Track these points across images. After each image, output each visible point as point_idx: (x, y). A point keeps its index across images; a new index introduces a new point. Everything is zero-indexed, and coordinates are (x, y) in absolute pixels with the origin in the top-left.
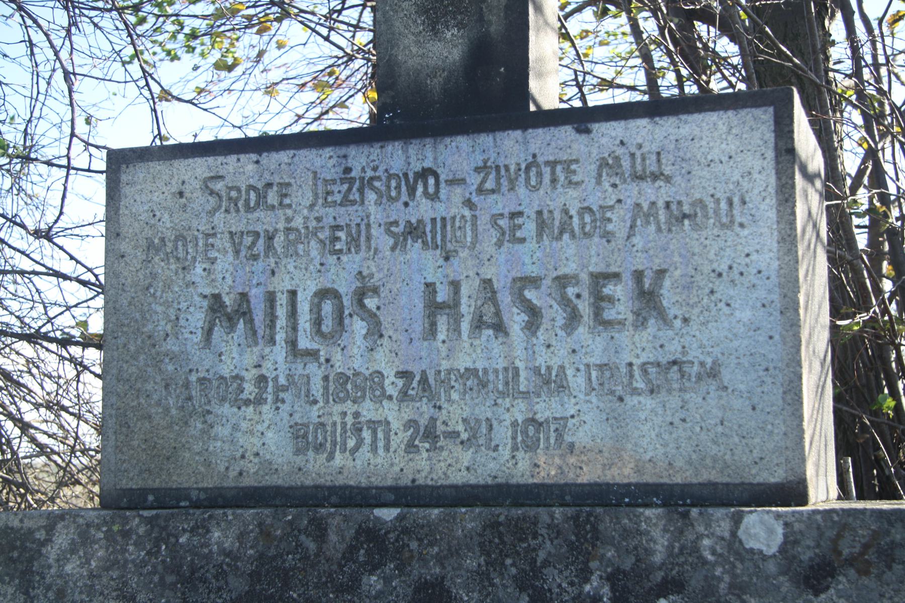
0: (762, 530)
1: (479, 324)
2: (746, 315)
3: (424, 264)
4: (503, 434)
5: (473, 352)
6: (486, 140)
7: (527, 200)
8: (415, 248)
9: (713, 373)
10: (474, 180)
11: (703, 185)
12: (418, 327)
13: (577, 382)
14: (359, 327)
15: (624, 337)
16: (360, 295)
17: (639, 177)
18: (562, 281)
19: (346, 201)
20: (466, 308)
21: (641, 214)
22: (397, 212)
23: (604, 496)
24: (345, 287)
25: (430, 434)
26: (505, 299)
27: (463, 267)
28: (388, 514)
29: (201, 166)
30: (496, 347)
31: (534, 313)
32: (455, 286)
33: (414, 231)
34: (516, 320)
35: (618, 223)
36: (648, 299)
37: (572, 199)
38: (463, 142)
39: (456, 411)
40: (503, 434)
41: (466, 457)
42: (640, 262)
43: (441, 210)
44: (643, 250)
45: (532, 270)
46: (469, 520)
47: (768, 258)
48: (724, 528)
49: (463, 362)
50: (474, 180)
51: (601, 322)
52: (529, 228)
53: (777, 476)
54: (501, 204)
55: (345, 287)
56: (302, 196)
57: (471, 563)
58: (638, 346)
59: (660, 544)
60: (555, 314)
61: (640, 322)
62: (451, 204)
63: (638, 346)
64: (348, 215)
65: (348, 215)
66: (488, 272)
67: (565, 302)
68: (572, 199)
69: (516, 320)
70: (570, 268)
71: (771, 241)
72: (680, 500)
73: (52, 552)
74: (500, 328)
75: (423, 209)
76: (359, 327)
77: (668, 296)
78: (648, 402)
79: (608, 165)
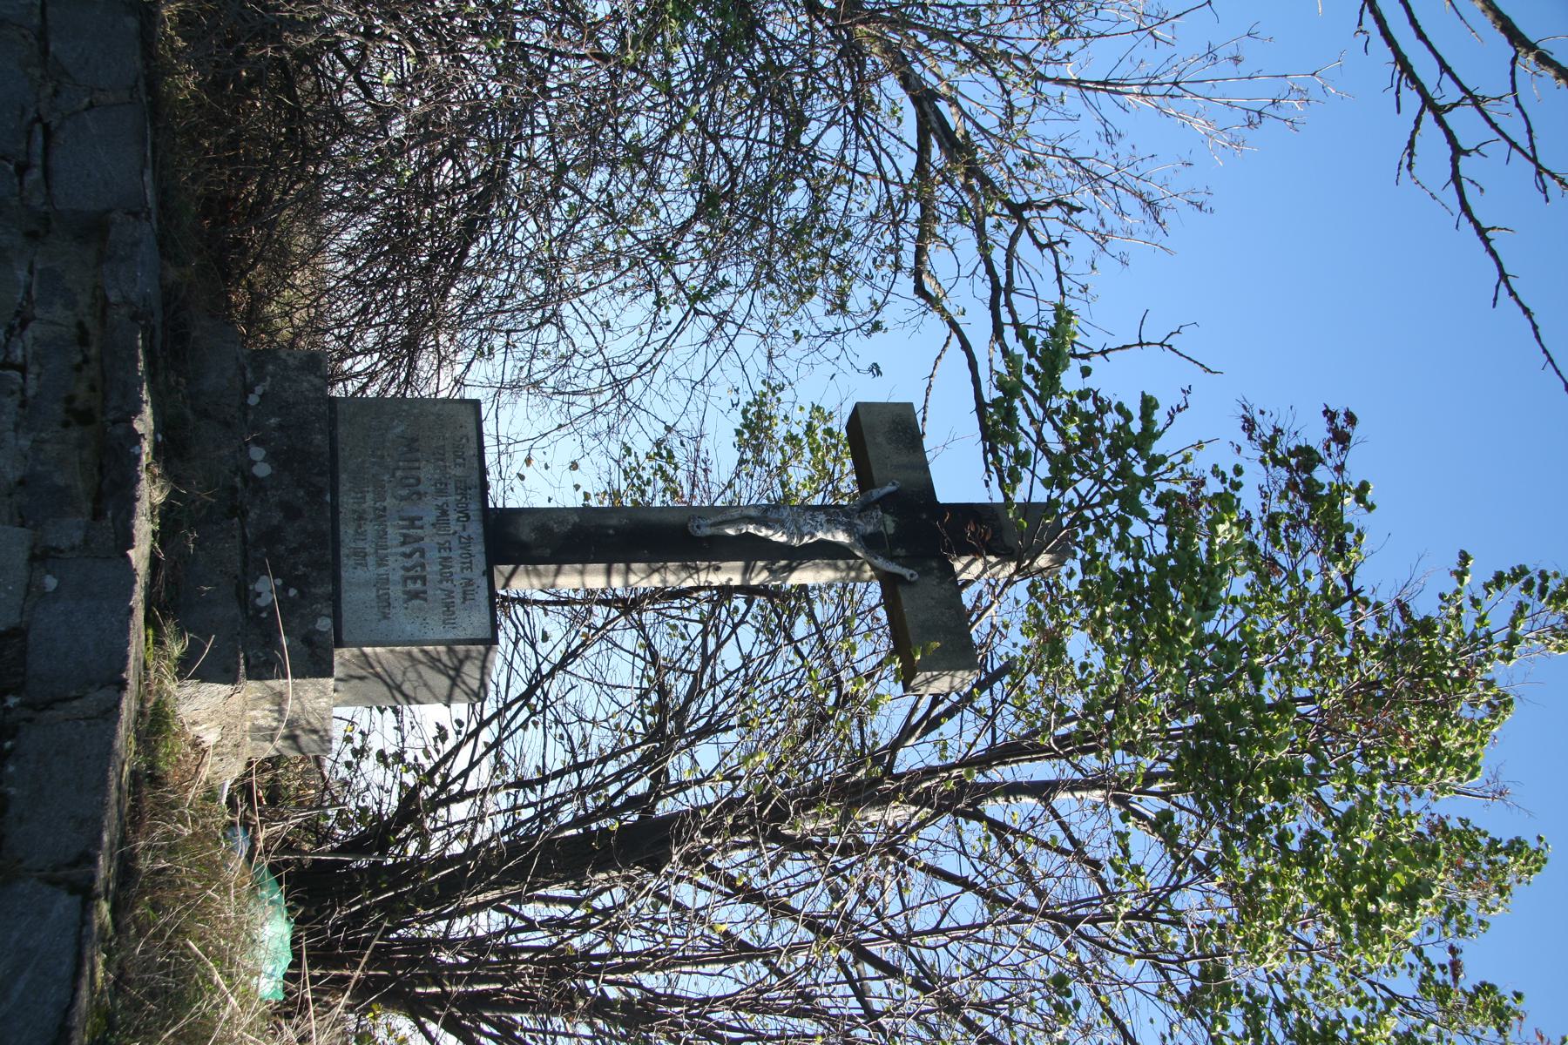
0: (324, 624)
1: (405, 536)
2: (409, 628)
3: (431, 516)
4: (361, 544)
5: (393, 533)
6: (481, 539)
7: (456, 554)
8: (438, 513)
9: (386, 617)
10: (465, 534)
11: (461, 615)
12: (404, 514)
13: (382, 570)
14: (405, 492)
15: (400, 587)
16: (418, 493)
17: (464, 593)
18: (423, 566)
19: (457, 488)
20: (412, 532)
21: (450, 594)
22: (452, 507)
23: (336, 579)
24: (421, 488)
25: (360, 518)
26: (416, 545)
27: (429, 530)
28: (328, 498)
29: (473, 434)
30: (395, 543)
31: (409, 556)
32: (422, 528)
33: (444, 513)
34: (407, 549)
35: (445, 585)
36: (415, 595)
37: (456, 569)
38: (481, 531)
39: (370, 529)
40: (361, 544)
41: (351, 532)
42: (430, 592)
43: (453, 523)
44: (436, 593)
45: (428, 555)
46: (326, 526)
47: (431, 636)
48: (325, 611)
49: (390, 530)
50: (465, 534)
51: (405, 580)
52: (445, 554)
53: (345, 637)
54: (455, 543)
55: (421, 488)
56: (458, 472)
57: (310, 527)
58: (396, 592)
59: (319, 591)
60: (409, 563)
61: (405, 592)
62: (455, 527)
63: (396, 592)
64: (451, 487)
65: (451, 487)
66: (427, 540)
67: (414, 567)
68: (456, 569)
69: (407, 549)
70: (428, 568)
71: (437, 637)
72: (335, 600)
73: (312, 378)
74: (403, 544)
75: (453, 516)
76: (405, 492)
77: (417, 602)
78: (374, 595)
79: (470, 582)
